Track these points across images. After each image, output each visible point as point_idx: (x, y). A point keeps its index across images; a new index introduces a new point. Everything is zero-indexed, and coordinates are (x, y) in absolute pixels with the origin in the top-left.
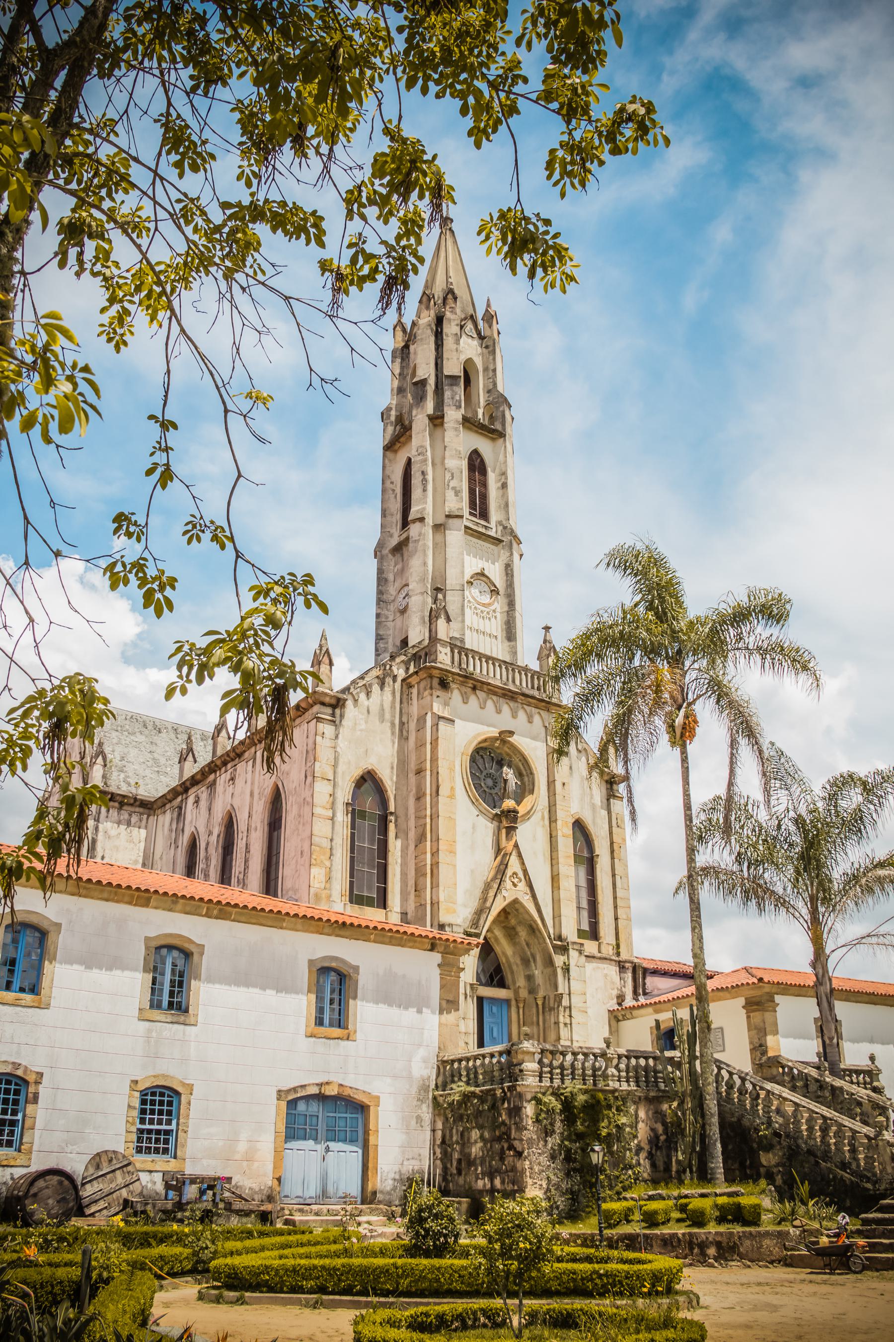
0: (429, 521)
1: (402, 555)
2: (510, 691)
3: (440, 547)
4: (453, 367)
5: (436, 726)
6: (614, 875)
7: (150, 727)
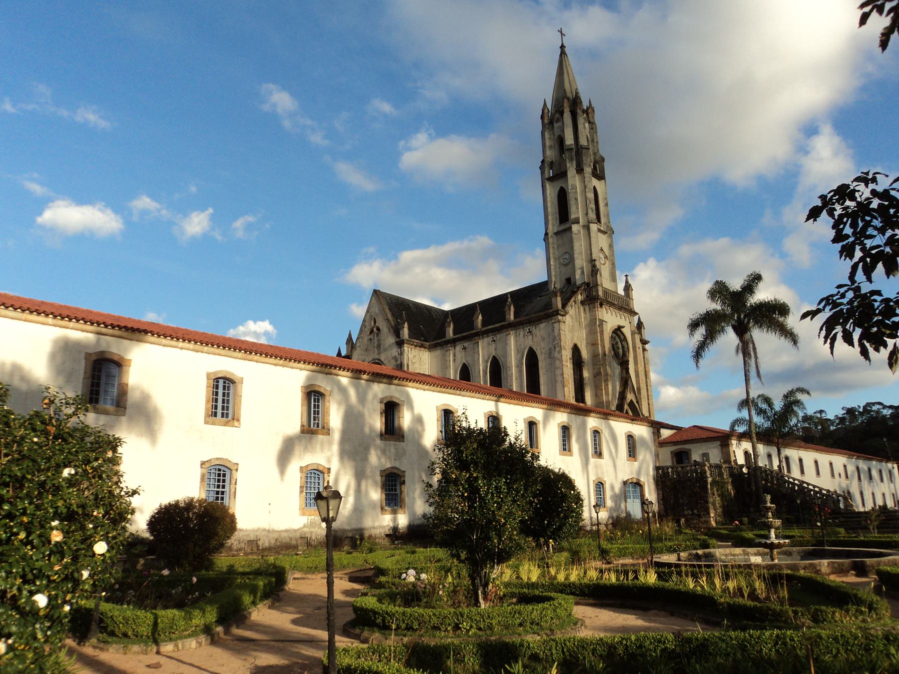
4: (583, 142)
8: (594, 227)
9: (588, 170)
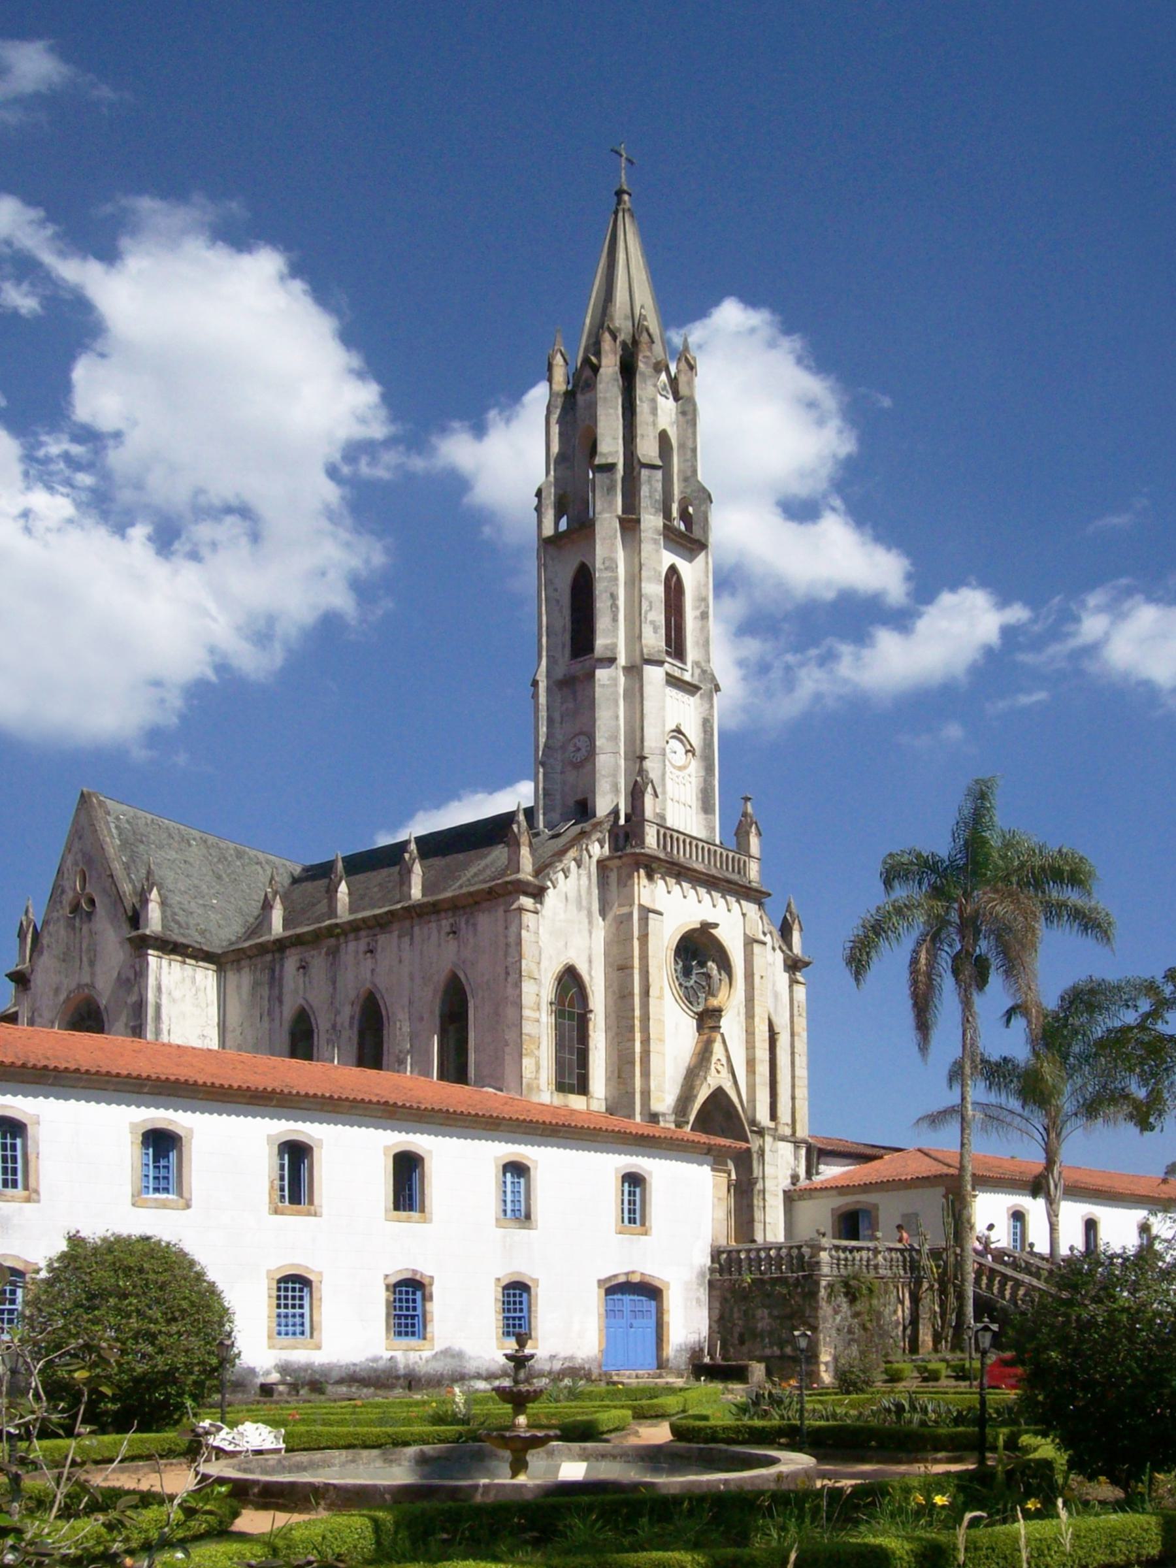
0: (622, 661)
1: (574, 693)
2: (713, 877)
3: (635, 694)
4: (648, 449)
5: (644, 921)
6: (793, 1054)
7: (177, 838)
8: (654, 675)
9: (651, 521)
